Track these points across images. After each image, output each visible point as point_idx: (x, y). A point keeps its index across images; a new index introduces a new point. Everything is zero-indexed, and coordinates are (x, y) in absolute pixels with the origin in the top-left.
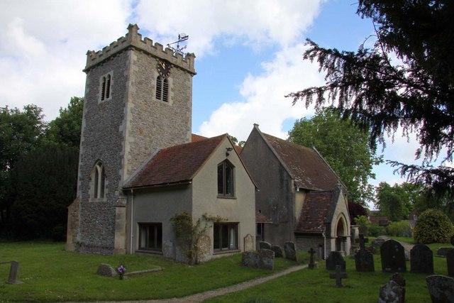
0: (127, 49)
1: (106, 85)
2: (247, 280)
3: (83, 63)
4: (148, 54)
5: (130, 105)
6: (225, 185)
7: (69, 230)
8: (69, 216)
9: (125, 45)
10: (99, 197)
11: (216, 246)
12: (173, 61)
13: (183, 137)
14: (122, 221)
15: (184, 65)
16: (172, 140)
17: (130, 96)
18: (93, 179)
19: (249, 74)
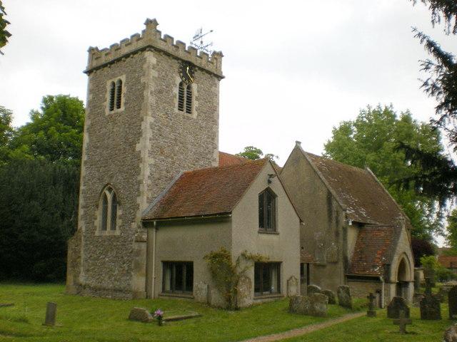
0: (143, 50)
1: (116, 92)
2: (299, 326)
3: (84, 62)
4: (168, 54)
6: (267, 220)
7: (69, 269)
8: (70, 252)
9: (141, 44)
11: (257, 290)
12: (197, 62)
15: (210, 68)
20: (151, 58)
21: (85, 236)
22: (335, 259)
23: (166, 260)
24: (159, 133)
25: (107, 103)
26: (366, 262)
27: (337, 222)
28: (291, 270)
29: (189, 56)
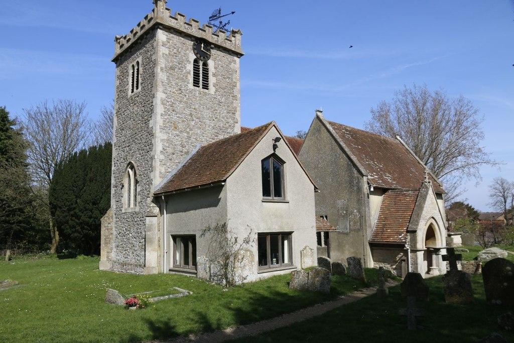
5: (160, 95)
6: (272, 183)
10: (132, 205)
11: (263, 260)
13: (229, 130)
14: (154, 235)
16: (217, 134)
17: (159, 84)
18: (126, 186)
20: (161, 35)
24: (171, 108)
29: (203, 33)
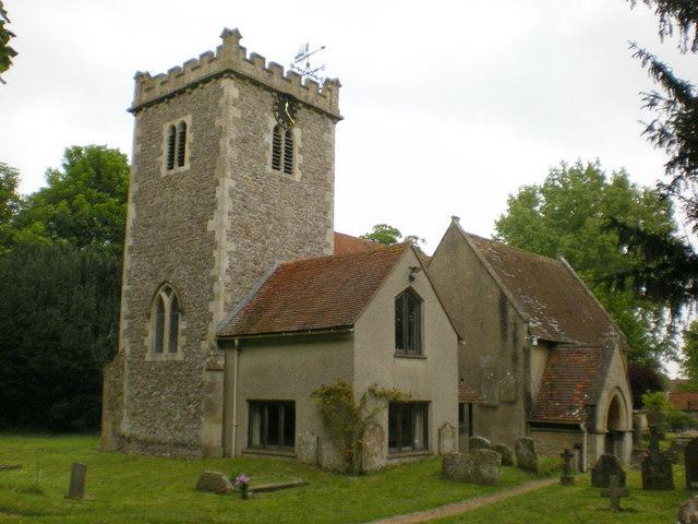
0: (219, 76)
1: (178, 141)
2: (457, 500)
3: (128, 95)
4: (256, 83)
6: (408, 337)
7: (106, 412)
8: (106, 386)
9: (215, 68)
11: (392, 444)
12: (301, 95)
15: (321, 104)
19: (62, 171)
20: (230, 89)
21: (130, 362)
22: (512, 397)
23: (254, 398)
24: (243, 205)
25: (164, 158)
26: (559, 401)
27: (515, 340)
28: (444, 413)
29: (289, 85)
